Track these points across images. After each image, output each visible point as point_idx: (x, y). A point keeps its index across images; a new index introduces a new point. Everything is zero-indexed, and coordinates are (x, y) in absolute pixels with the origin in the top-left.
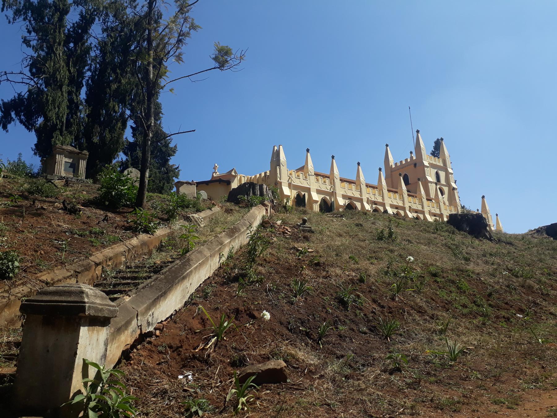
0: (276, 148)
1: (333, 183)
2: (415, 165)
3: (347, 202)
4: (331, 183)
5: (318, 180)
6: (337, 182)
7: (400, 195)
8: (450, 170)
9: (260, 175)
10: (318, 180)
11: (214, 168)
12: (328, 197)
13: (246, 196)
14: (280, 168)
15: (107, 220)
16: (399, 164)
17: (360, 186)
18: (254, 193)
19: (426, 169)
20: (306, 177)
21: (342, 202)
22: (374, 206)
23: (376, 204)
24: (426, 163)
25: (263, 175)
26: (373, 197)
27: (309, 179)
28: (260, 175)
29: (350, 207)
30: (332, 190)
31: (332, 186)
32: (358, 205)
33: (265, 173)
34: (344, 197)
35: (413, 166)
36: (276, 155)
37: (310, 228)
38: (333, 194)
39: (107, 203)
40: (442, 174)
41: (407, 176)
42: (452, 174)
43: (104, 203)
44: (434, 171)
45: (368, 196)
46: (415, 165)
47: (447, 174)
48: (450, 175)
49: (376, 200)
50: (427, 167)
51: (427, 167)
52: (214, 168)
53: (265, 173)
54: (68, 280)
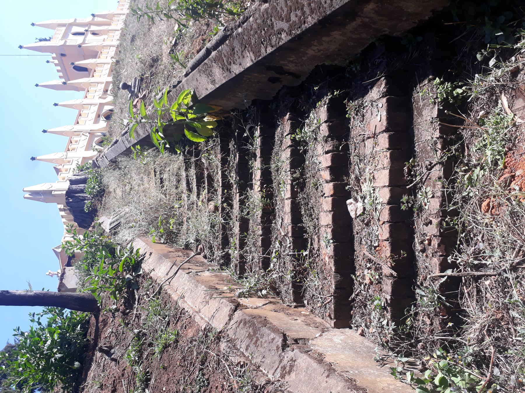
0: (27, 195)
1: (77, 133)
2: (63, 55)
3: (102, 118)
4: (78, 135)
5: (73, 149)
6: (77, 128)
7: (97, 66)
8: (72, 21)
9: (63, 217)
10: (73, 149)
11: (52, 276)
12: (96, 139)
13: (86, 201)
14: (55, 191)
15: (111, 348)
16: (61, 74)
17: (84, 105)
18: (82, 191)
19: (67, 44)
20: (69, 162)
21: (103, 124)
22: (109, 92)
23: (107, 91)
24: (62, 43)
25: (63, 213)
26: (97, 93)
27: (72, 158)
28: (63, 217)
29: (108, 117)
30: (87, 134)
31: (81, 133)
32: (107, 108)
33: (61, 210)
34: (96, 121)
35: (63, 58)
36: (36, 195)
37: (136, 79)
38: (92, 134)
39: (77, 364)
40: (75, 29)
41: (74, 64)
42: (76, 20)
43: (74, 371)
44: (71, 36)
45: (97, 98)
46: (63, 55)
47: (75, 24)
48: (77, 22)
49: (102, 90)
50: (66, 42)
51: (66, 42)
52: (52, 276)
53: (61, 210)
54: (328, 359)
